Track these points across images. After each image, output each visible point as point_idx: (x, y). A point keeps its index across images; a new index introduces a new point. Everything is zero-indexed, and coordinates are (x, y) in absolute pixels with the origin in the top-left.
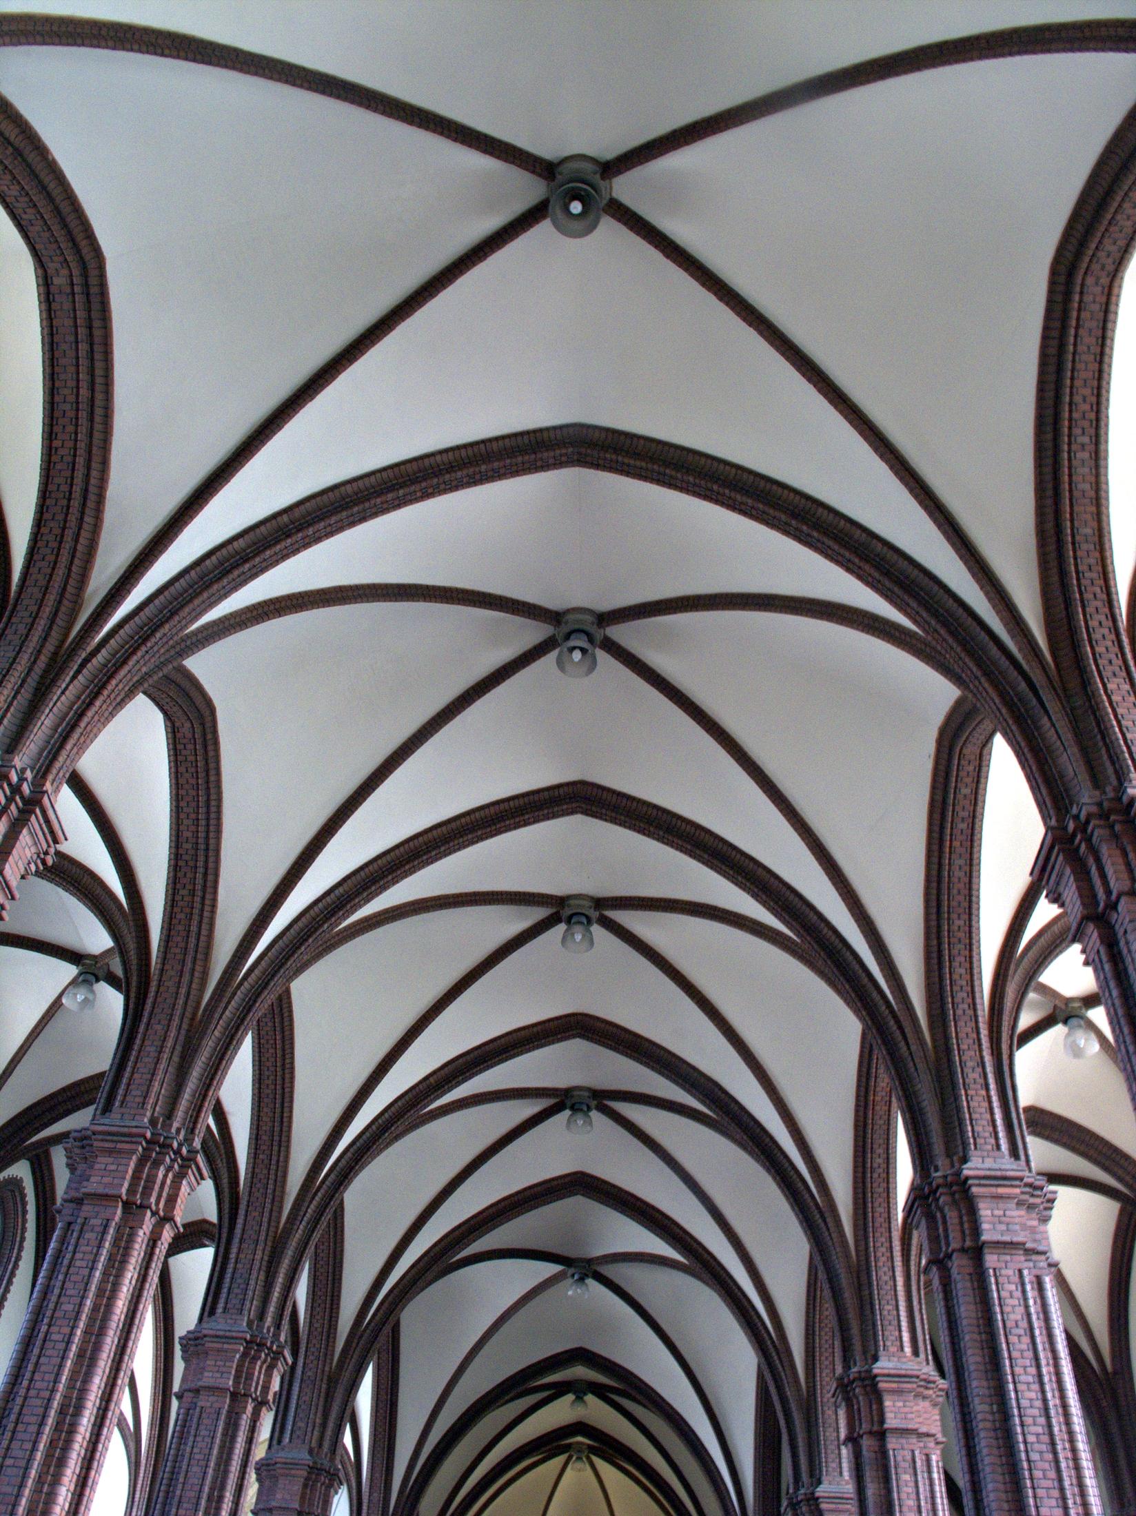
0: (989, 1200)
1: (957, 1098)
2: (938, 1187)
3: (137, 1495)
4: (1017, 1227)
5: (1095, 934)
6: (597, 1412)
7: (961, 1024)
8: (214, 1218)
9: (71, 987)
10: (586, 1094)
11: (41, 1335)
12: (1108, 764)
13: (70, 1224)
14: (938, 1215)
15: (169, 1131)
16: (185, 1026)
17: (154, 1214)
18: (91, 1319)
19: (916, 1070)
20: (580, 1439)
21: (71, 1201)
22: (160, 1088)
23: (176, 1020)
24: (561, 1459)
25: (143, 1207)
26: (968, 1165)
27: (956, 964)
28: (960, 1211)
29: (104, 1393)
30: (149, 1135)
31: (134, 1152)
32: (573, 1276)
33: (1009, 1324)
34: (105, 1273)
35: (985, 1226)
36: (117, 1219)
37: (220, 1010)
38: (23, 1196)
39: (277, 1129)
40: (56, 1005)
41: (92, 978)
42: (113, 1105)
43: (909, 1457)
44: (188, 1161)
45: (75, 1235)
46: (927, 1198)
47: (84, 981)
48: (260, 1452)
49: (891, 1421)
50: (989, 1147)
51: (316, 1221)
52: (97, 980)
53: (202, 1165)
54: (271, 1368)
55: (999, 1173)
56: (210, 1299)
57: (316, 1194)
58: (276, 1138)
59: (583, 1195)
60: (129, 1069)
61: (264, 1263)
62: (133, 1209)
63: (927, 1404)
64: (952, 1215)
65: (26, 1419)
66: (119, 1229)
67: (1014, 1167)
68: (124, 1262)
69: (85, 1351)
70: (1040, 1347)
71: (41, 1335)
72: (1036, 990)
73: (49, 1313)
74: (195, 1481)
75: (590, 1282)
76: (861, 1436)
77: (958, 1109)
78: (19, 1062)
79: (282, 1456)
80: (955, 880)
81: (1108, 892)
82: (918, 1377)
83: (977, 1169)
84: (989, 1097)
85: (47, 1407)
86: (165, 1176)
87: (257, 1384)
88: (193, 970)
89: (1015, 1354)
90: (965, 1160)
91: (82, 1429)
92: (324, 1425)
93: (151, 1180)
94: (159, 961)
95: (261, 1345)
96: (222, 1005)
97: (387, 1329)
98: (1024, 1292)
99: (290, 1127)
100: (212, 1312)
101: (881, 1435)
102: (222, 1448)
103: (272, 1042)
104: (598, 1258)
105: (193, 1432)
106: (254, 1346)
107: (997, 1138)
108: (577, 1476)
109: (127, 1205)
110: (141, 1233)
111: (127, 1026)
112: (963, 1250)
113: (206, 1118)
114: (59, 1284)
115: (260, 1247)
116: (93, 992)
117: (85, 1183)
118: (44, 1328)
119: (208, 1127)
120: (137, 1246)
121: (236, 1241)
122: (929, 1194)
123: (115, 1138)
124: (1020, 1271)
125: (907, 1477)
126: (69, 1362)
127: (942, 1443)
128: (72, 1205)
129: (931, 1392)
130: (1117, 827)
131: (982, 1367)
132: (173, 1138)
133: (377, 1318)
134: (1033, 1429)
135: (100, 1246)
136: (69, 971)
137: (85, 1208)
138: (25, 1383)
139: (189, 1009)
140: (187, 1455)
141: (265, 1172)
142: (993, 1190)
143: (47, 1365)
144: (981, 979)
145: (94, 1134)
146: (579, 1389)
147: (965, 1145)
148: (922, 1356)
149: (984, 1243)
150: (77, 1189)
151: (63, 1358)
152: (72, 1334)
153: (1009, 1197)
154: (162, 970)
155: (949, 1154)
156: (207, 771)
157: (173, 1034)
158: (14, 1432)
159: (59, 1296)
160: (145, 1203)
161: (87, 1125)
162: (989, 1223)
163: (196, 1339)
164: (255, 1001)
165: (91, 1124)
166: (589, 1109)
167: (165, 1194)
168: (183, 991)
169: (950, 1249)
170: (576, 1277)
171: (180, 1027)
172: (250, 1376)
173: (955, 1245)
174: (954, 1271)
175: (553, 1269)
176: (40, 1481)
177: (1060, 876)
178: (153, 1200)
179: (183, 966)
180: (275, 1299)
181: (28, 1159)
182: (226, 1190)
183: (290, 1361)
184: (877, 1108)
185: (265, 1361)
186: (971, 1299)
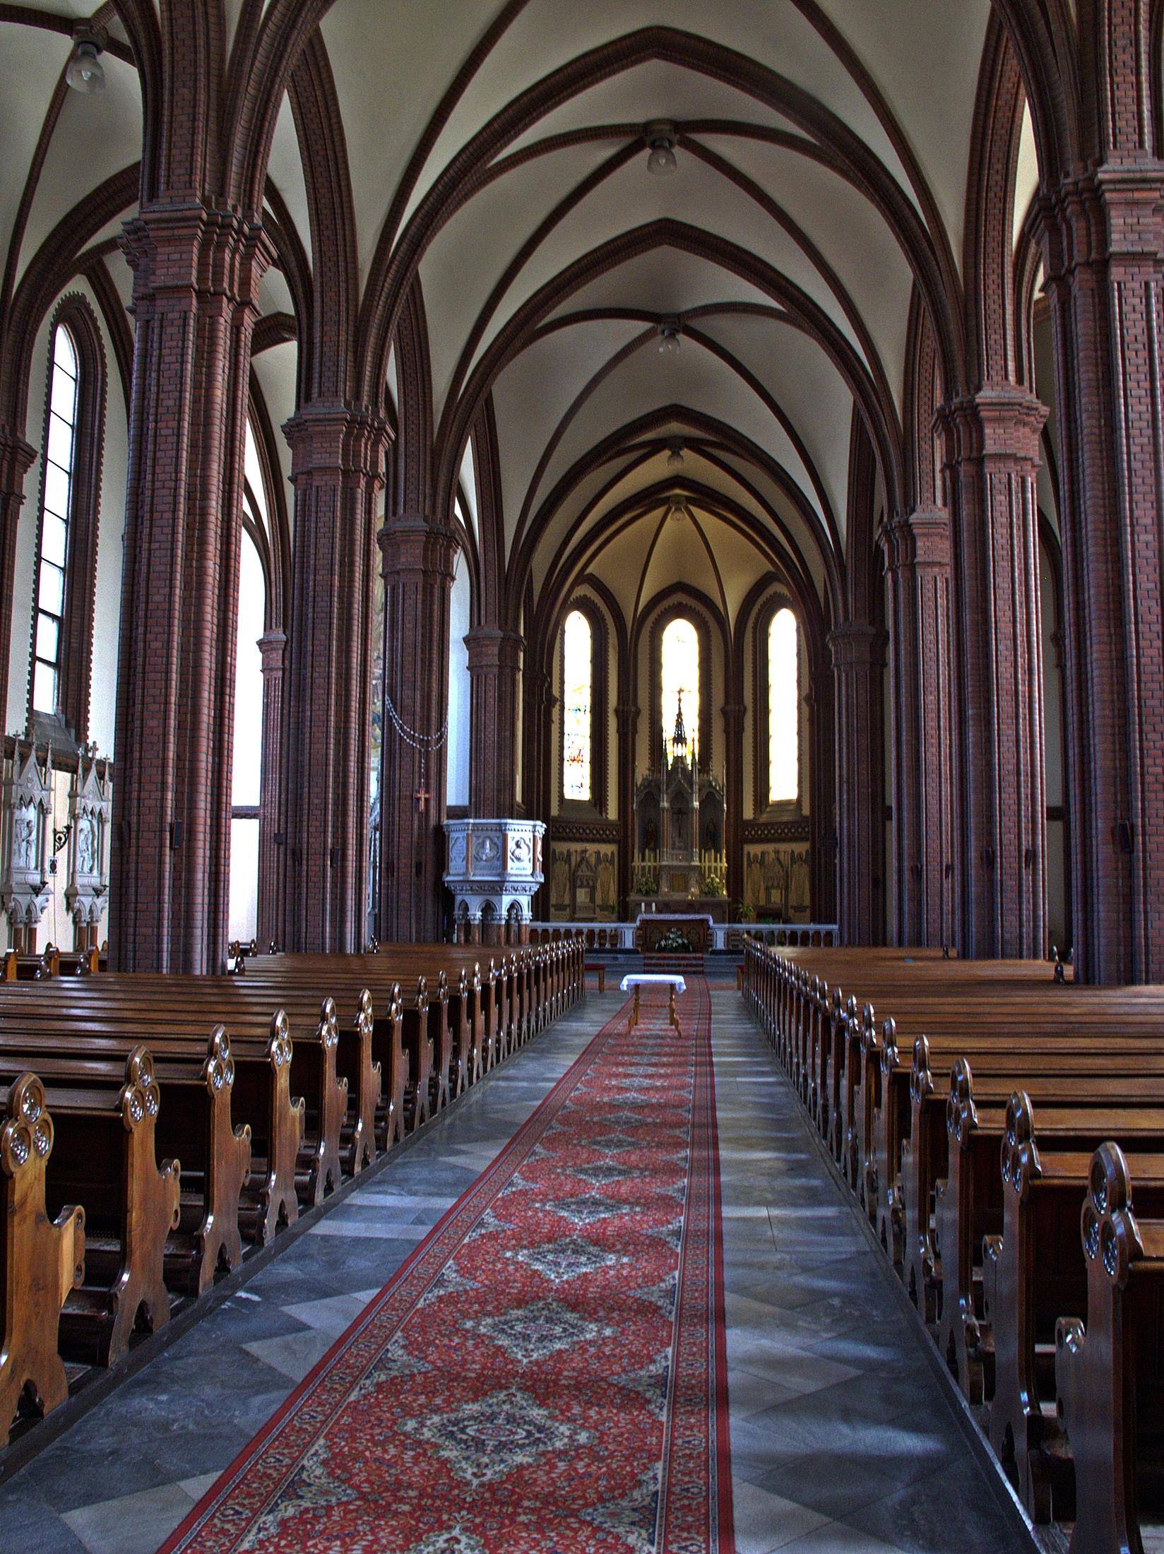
0: (1123, 207)
1: (1100, 88)
2: (1067, 195)
3: (273, 577)
4: (1151, 236)
6: (693, 464)
8: (291, 311)
9: (71, 64)
10: (667, 127)
11: (151, 433)
13: (148, 322)
14: (1064, 227)
15: (225, 209)
16: (213, 86)
17: (230, 300)
19: (1055, 56)
20: (677, 491)
21: (142, 298)
22: (203, 162)
23: (202, 82)
24: (659, 512)
25: (219, 294)
26: (1105, 167)
28: (1088, 221)
29: (224, 477)
30: (204, 216)
31: (194, 236)
32: (663, 332)
33: (1127, 339)
34: (197, 366)
35: (1115, 236)
36: (194, 309)
37: (248, 62)
38: (91, 313)
39: (337, 200)
40: (62, 89)
41: (93, 49)
42: (158, 189)
43: (1005, 480)
44: (252, 241)
45: (157, 331)
46: (1053, 209)
47: (85, 53)
48: (379, 524)
49: (990, 447)
50: (1131, 145)
51: (394, 296)
52: (99, 51)
53: (267, 242)
55: (1138, 175)
56: (303, 386)
57: (390, 267)
58: (338, 211)
59: (670, 244)
60: (164, 146)
61: (350, 344)
62: (208, 298)
63: (1027, 430)
64: (1078, 227)
65: (160, 508)
66: (198, 320)
67: (1157, 167)
69: (197, 440)
71: (151, 433)
73: (152, 411)
74: (324, 550)
75: (681, 337)
76: (960, 464)
77: (1100, 102)
78: (42, 163)
79: (399, 526)
82: (1020, 405)
83: (1115, 171)
84: (1139, 83)
85: (176, 496)
86: (233, 259)
87: (366, 459)
89: (1129, 369)
90: (1101, 162)
91: (213, 511)
92: (434, 495)
93: (219, 265)
94: (164, 7)
95: (363, 423)
96: (250, 54)
97: (481, 402)
98: (1148, 305)
100: (308, 398)
101: (979, 461)
102: (343, 519)
103: (312, 99)
104: (687, 312)
105: (313, 509)
106: (356, 425)
107: (1141, 134)
108: (675, 525)
109: (201, 294)
110: (222, 320)
111: (150, 96)
112: (1087, 264)
113: (260, 200)
114: (154, 382)
115: (343, 328)
116: (98, 66)
117: (152, 278)
118: (152, 425)
119: (265, 211)
120: (221, 335)
121: (317, 325)
122: (1057, 203)
123: (170, 225)
124: (1147, 284)
126: (185, 454)
127: (1039, 466)
128: (145, 302)
129: (1032, 419)
131: (1093, 383)
132: (231, 217)
133: (471, 390)
135: (184, 339)
136: (64, 44)
137: (158, 302)
138: (149, 477)
139: (213, 65)
140: (313, 530)
141: (333, 248)
142: (1130, 195)
143: (165, 457)
145: (147, 223)
146: (674, 445)
147: (1103, 145)
148: (1026, 383)
149: (1111, 255)
150: (146, 285)
151: (178, 450)
152: (180, 427)
153: (1146, 203)
154: (171, 19)
155: (1083, 158)
157: (202, 97)
158: (151, 520)
159: (158, 393)
160: (219, 289)
161: (137, 216)
162: (1120, 232)
163: (298, 425)
164: (285, 46)
165: (140, 213)
166: (671, 144)
167: (236, 278)
168: (201, 42)
169: (1073, 264)
170: (666, 333)
171: (209, 74)
172: (357, 454)
173: (1078, 257)
174: (1075, 290)
175: (643, 326)
176: (187, 558)
178: (226, 285)
179: (193, 10)
180: (367, 378)
181: (82, 273)
182: (296, 273)
183: (393, 436)
184: (1000, 115)
185: (369, 438)
186: (1090, 316)
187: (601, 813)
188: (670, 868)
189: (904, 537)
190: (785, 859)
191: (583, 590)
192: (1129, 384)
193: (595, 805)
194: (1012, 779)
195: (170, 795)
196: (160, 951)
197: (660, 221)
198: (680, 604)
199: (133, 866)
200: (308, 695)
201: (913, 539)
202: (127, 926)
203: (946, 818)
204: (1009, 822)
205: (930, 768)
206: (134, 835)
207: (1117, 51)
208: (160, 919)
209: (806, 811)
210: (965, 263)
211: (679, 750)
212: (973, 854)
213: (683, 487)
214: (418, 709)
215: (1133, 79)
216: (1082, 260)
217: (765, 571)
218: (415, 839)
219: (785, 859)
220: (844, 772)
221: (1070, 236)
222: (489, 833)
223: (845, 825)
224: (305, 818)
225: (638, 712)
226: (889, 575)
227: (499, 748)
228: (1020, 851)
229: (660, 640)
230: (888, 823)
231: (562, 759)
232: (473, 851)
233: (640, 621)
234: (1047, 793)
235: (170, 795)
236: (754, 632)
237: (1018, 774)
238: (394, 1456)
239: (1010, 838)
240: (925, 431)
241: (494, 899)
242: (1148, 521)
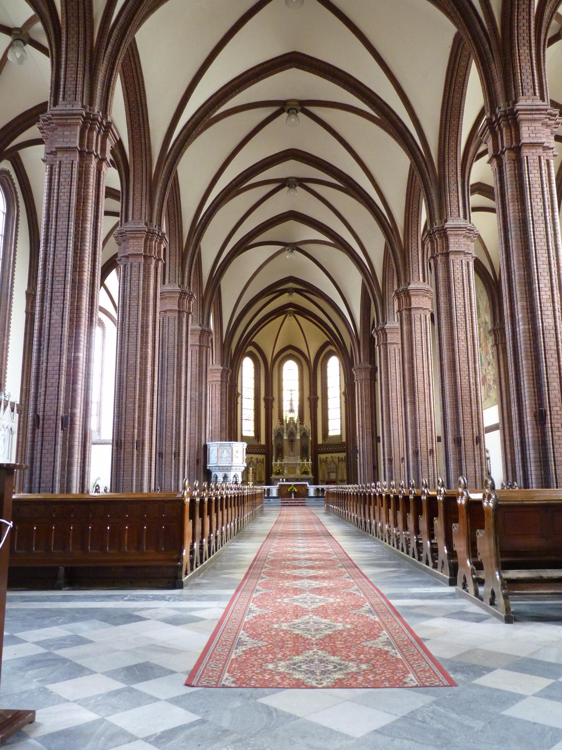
5: (496, 163)
7: (451, 166)
10: (295, 180)
11: (128, 304)
12: (513, 89)
17: (96, 157)
18: (143, 297)
20: (290, 309)
24: (283, 316)
27: (451, 141)
33: (455, 279)
39: (176, 211)
43: (419, 316)
45: (129, 269)
54: (190, 301)
55: (458, 226)
58: (176, 214)
63: (427, 298)
68: (149, 276)
70: (465, 286)
72: (473, 192)
75: (295, 252)
76: (403, 310)
80: (454, 104)
81: (503, 147)
86: (155, 244)
88: (146, 159)
99: (181, 209)
108: (290, 321)
112: (442, 254)
117: (127, 250)
124: (462, 261)
125: (418, 323)
130: (510, 121)
134: (459, 312)
142: (455, 232)
144: (460, 146)
146: (290, 291)
148: (426, 282)
155: (441, 218)
156: (136, 69)
174: (439, 261)
175: (279, 248)
177: (488, 137)
184: (416, 188)
187: (258, 441)
188: (288, 464)
189: (383, 334)
190: (336, 461)
191: (251, 348)
192: (456, 293)
193: (256, 438)
194: (424, 423)
195: (136, 430)
196: (132, 485)
197: (290, 211)
198: (290, 354)
199: (122, 455)
200: (165, 395)
201: (386, 335)
202: (119, 477)
203: (401, 440)
204: (423, 439)
205: (394, 421)
206: (123, 444)
207: (451, 185)
208: (132, 474)
209: (344, 440)
210: (404, 239)
211: (291, 415)
212: (410, 451)
213: (293, 307)
214: (197, 399)
215: (456, 194)
216: (441, 252)
217: (325, 341)
218: (196, 450)
219: (336, 461)
220: (360, 423)
221: (437, 244)
222: (226, 447)
223: (361, 444)
224: (164, 441)
225: (273, 399)
226: (378, 348)
227: (221, 414)
228: (427, 449)
229: (282, 370)
230: (378, 443)
231: (242, 419)
232: (220, 455)
233: (274, 361)
234: (438, 431)
235: (136, 430)
236: (321, 366)
237: (426, 422)
238: (269, 678)
239: (424, 445)
240: (391, 299)
241: (228, 473)
242: (463, 338)
